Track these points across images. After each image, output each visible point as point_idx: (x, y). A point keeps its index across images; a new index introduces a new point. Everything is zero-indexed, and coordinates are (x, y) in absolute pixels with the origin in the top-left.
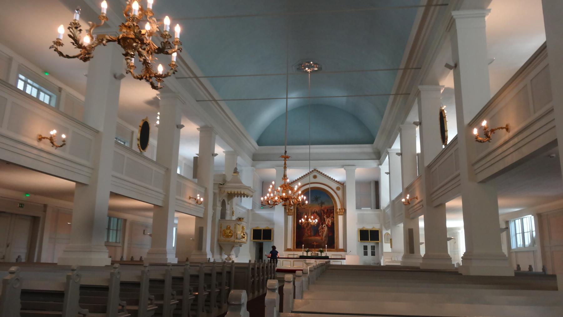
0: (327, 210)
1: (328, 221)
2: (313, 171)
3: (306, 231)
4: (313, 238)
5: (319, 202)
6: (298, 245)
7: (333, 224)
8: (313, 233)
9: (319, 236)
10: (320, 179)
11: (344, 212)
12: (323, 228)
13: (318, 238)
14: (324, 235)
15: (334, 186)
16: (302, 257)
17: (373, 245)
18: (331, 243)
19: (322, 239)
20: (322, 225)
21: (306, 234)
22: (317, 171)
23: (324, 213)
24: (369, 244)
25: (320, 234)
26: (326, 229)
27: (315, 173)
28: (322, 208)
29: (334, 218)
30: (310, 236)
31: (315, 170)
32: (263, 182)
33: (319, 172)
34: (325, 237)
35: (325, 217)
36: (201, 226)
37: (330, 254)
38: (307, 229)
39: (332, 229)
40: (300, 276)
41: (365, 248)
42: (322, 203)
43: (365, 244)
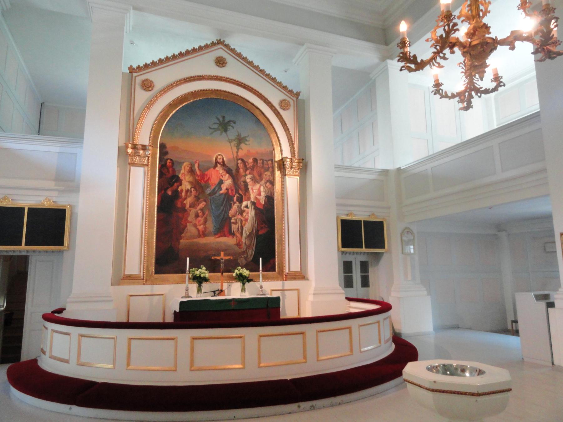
0: (255, 160)
1: (257, 192)
2: (213, 44)
3: (191, 218)
4: (211, 240)
5: (232, 133)
6: (168, 258)
7: (270, 199)
8: (211, 226)
9: (232, 234)
10: (234, 69)
11: (304, 166)
12: (241, 212)
13: (230, 241)
14: (248, 228)
15: (275, 97)
16: (191, 316)
17: (364, 258)
18: (264, 251)
19: (239, 244)
20: (240, 201)
21: (191, 229)
22: (227, 46)
23: (246, 169)
24: (357, 255)
25: (234, 227)
26: (251, 214)
27: (220, 52)
28: (241, 153)
29: (272, 183)
30: (204, 234)
31: (219, 42)
32: (42, 104)
33: (233, 51)
34: (249, 236)
35: (248, 179)
36: (365, 289)
37: (264, 287)
38: (193, 212)
39: (267, 215)
40: (487, 91)
41: (347, 267)
42: (240, 140)
43: (348, 258)
